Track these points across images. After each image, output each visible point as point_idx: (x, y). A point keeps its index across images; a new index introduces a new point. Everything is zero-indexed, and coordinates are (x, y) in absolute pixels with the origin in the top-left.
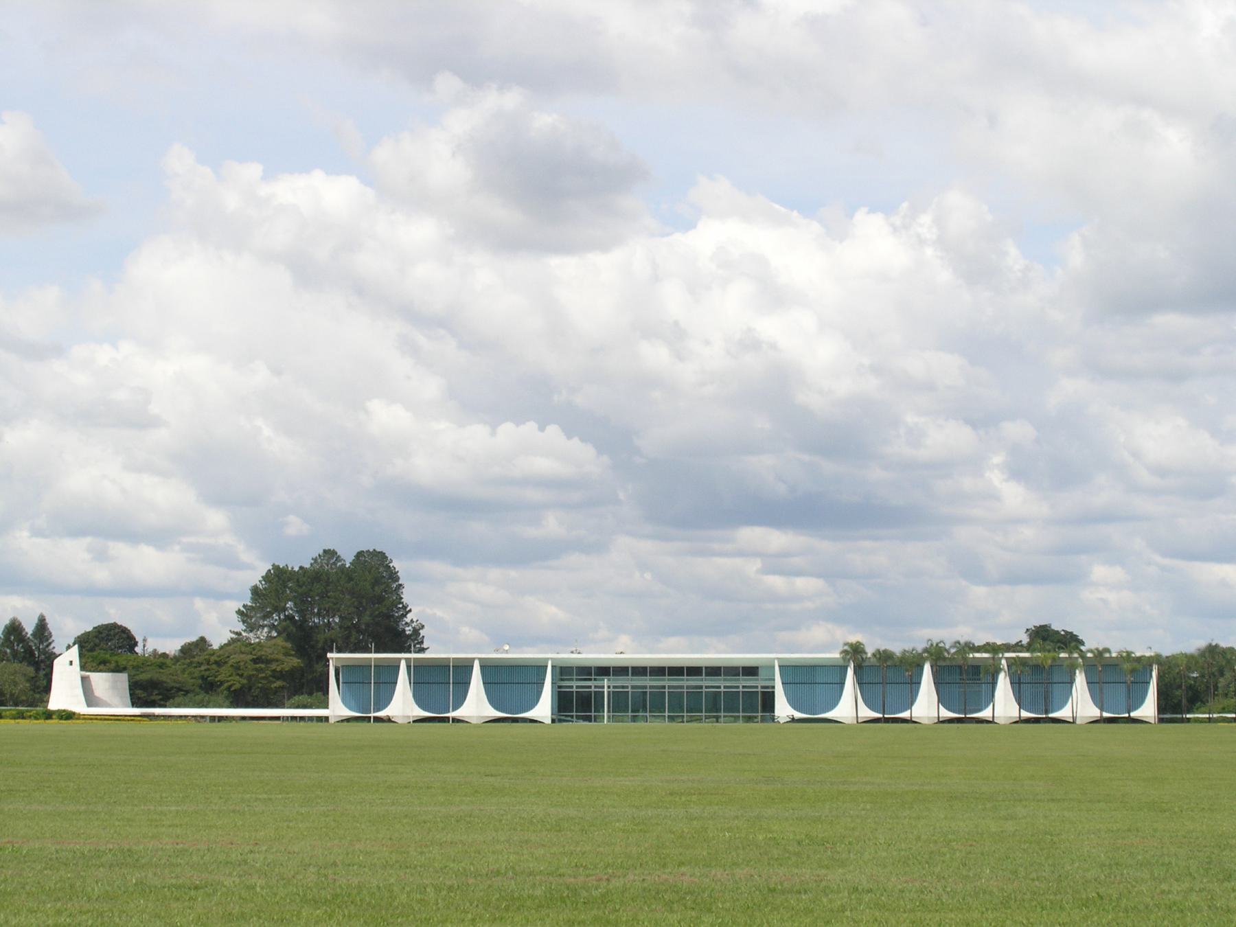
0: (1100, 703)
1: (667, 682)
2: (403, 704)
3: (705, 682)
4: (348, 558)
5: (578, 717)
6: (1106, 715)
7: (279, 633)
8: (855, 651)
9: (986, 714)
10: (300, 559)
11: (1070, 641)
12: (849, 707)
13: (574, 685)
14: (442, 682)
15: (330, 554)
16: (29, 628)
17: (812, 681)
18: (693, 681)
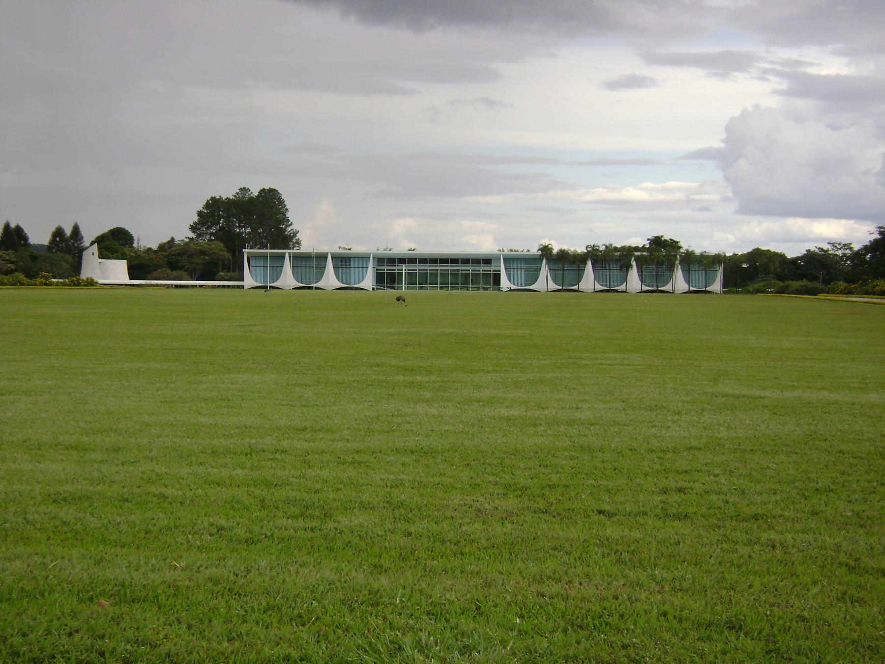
0: (688, 281)
1: (439, 267)
2: (288, 279)
3: (460, 267)
4: (255, 193)
5: (388, 287)
6: (692, 289)
7: (216, 239)
8: (546, 251)
9: (668, 288)
10: (228, 191)
11: (673, 245)
12: (545, 281)
13: (386, 268)
14: (310, 264)
15: (244, 190)
16: (68, 232)
17: (525, 265)
18: (455, 267)
